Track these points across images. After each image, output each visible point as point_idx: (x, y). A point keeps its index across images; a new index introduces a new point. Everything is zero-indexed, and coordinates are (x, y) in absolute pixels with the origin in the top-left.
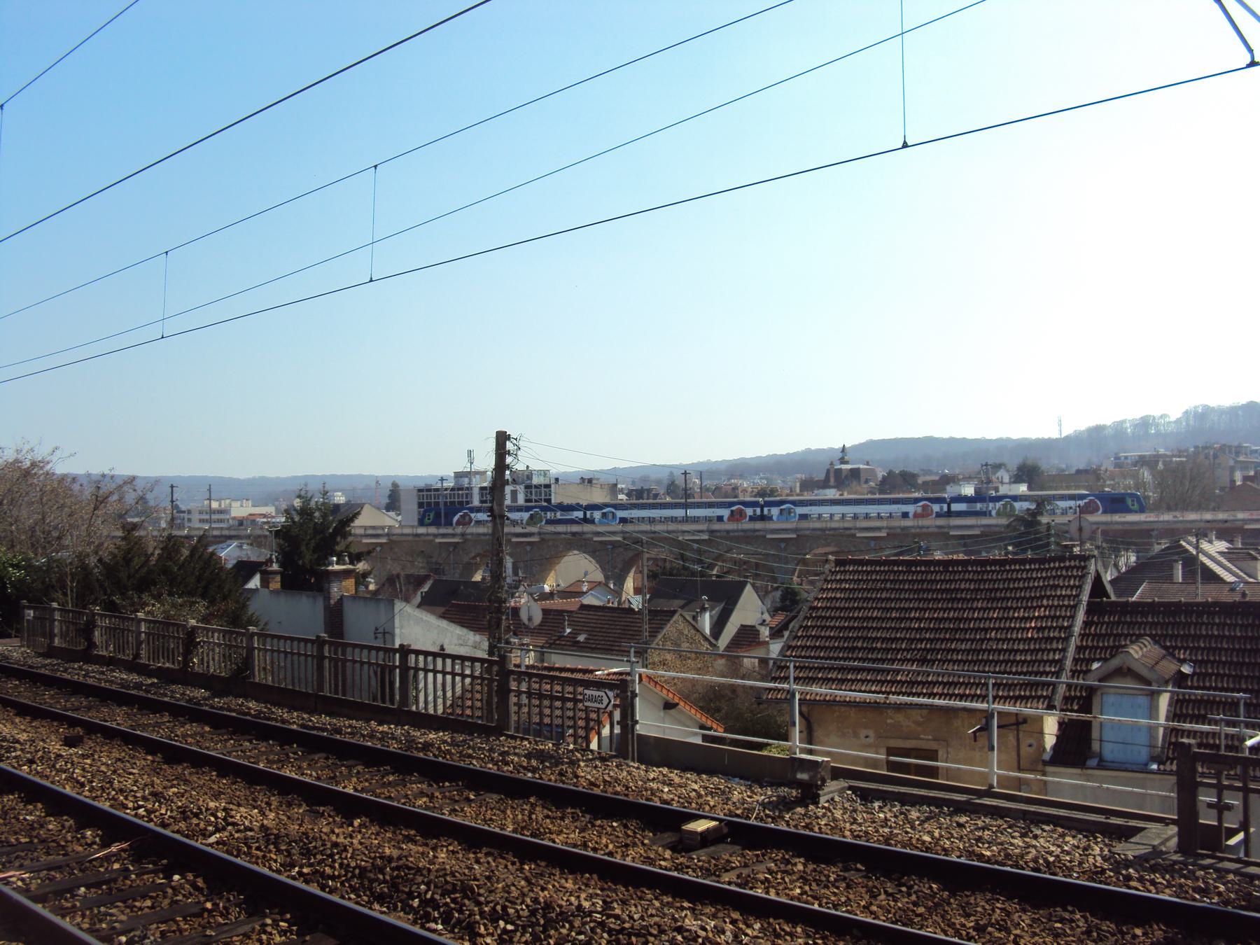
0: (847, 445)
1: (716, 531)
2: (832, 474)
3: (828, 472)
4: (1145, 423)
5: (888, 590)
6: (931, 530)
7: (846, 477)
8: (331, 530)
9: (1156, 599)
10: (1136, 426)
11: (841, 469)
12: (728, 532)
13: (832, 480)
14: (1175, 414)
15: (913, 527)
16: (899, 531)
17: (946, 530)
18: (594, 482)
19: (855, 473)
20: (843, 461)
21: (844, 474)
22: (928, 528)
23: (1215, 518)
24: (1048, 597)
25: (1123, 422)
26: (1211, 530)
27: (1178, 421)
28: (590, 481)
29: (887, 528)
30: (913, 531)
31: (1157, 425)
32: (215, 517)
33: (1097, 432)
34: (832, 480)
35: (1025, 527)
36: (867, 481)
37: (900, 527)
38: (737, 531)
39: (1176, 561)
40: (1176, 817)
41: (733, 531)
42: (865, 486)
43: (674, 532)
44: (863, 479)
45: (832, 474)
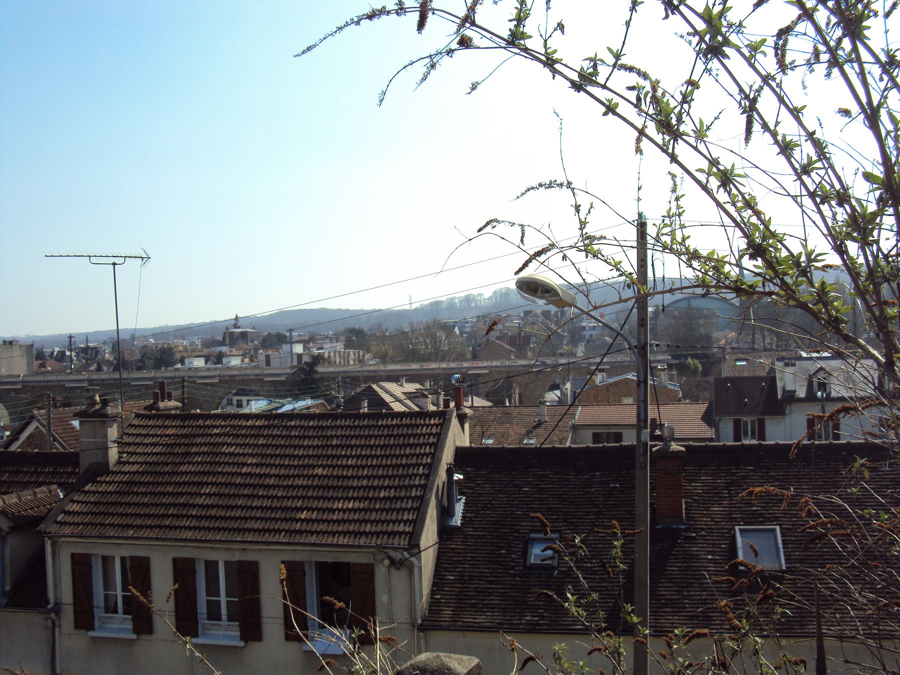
0: (240, 315)
1: (94, 380)
2: (227, 336)
3: (225, 334)
4: (468, 299)
5: (397, 457)
6: (251, 377)
7: (238, 338)
8: (675, 527)
9: (506, 446)
10: (461, 301)
11: (233, 332)
12: (103, 380)
13: (227, 340)
14: (488, 293)
15: (237, 375)
16: (228, 378)
17: (262, 377)
18: (14, 343)
19: (244, 335)
20: (236, 327)
21: (236, 336)
22: (249, 376)
23: (448, 367)
24: (411, 446)
25: (454, 298)
26: (404, 376)
27: (490, 298)
28: (11, 343)
29: (219, 376)
30: (238, 378)
31: (476, 301)
32: (538, 583)
33: (436, 304)
34: (227, 340)
35: (305, 375)
36: (252, 341)
37: (228, 376)
38: (110, 380)
39: (364, 400)
40: (237, 600)
41: (106, 380)
42: (250, 344)
43: (62, 381)
44: (250, 340)
45: (227, 336)
